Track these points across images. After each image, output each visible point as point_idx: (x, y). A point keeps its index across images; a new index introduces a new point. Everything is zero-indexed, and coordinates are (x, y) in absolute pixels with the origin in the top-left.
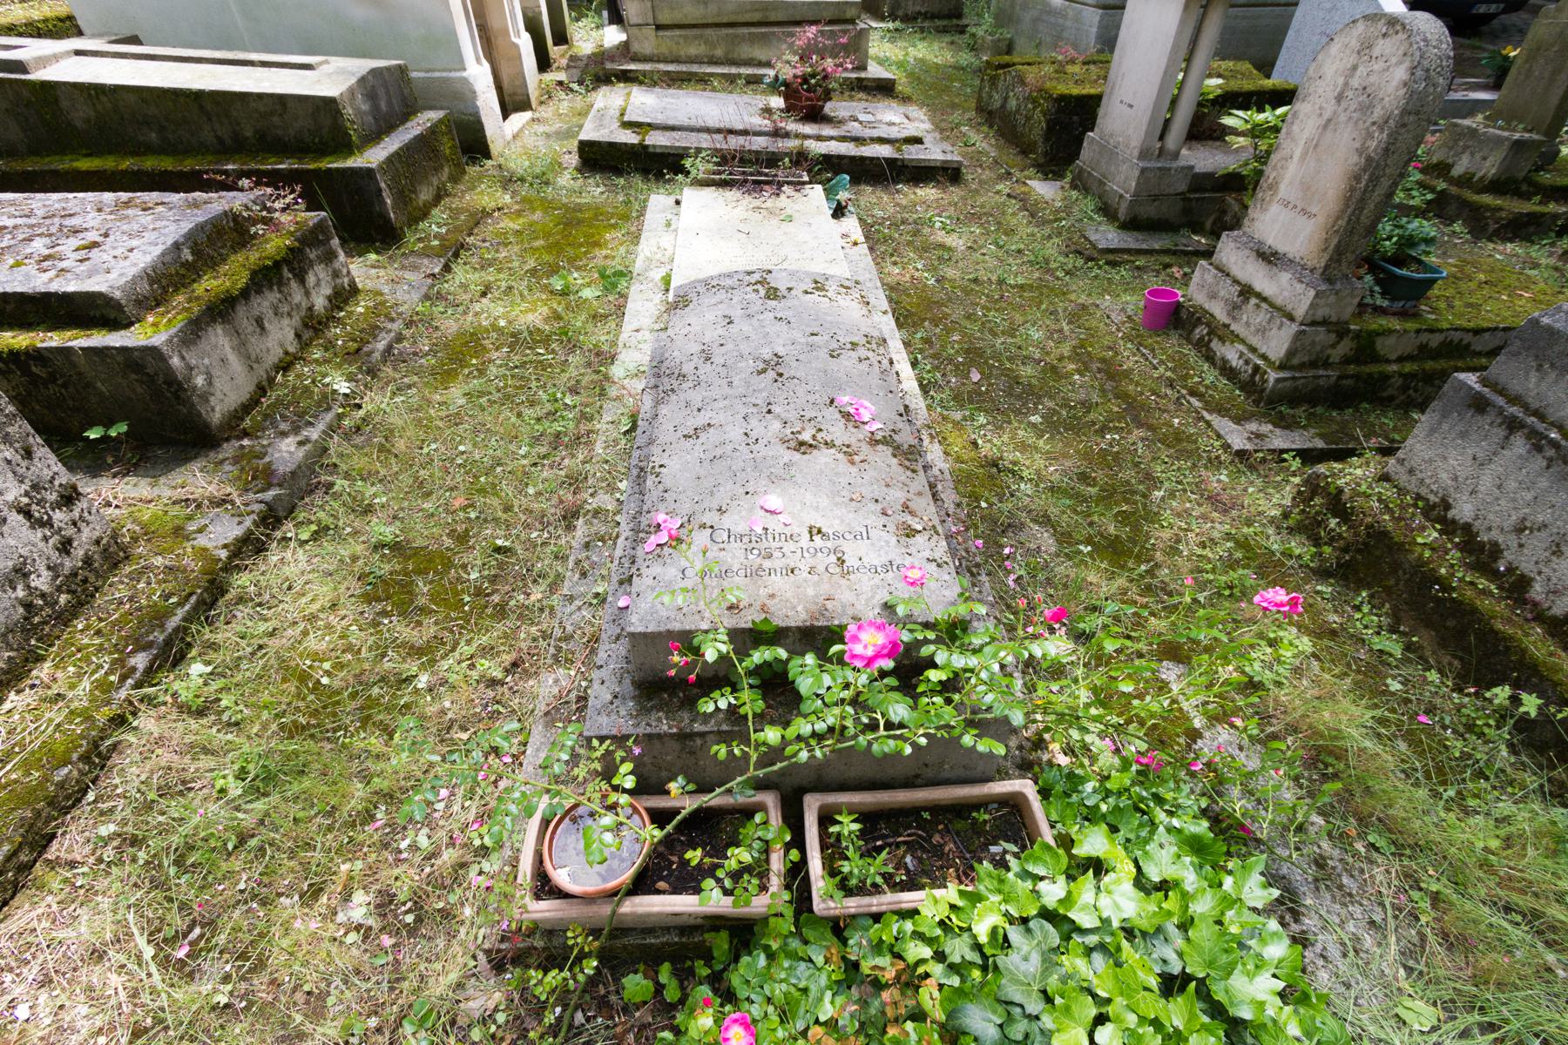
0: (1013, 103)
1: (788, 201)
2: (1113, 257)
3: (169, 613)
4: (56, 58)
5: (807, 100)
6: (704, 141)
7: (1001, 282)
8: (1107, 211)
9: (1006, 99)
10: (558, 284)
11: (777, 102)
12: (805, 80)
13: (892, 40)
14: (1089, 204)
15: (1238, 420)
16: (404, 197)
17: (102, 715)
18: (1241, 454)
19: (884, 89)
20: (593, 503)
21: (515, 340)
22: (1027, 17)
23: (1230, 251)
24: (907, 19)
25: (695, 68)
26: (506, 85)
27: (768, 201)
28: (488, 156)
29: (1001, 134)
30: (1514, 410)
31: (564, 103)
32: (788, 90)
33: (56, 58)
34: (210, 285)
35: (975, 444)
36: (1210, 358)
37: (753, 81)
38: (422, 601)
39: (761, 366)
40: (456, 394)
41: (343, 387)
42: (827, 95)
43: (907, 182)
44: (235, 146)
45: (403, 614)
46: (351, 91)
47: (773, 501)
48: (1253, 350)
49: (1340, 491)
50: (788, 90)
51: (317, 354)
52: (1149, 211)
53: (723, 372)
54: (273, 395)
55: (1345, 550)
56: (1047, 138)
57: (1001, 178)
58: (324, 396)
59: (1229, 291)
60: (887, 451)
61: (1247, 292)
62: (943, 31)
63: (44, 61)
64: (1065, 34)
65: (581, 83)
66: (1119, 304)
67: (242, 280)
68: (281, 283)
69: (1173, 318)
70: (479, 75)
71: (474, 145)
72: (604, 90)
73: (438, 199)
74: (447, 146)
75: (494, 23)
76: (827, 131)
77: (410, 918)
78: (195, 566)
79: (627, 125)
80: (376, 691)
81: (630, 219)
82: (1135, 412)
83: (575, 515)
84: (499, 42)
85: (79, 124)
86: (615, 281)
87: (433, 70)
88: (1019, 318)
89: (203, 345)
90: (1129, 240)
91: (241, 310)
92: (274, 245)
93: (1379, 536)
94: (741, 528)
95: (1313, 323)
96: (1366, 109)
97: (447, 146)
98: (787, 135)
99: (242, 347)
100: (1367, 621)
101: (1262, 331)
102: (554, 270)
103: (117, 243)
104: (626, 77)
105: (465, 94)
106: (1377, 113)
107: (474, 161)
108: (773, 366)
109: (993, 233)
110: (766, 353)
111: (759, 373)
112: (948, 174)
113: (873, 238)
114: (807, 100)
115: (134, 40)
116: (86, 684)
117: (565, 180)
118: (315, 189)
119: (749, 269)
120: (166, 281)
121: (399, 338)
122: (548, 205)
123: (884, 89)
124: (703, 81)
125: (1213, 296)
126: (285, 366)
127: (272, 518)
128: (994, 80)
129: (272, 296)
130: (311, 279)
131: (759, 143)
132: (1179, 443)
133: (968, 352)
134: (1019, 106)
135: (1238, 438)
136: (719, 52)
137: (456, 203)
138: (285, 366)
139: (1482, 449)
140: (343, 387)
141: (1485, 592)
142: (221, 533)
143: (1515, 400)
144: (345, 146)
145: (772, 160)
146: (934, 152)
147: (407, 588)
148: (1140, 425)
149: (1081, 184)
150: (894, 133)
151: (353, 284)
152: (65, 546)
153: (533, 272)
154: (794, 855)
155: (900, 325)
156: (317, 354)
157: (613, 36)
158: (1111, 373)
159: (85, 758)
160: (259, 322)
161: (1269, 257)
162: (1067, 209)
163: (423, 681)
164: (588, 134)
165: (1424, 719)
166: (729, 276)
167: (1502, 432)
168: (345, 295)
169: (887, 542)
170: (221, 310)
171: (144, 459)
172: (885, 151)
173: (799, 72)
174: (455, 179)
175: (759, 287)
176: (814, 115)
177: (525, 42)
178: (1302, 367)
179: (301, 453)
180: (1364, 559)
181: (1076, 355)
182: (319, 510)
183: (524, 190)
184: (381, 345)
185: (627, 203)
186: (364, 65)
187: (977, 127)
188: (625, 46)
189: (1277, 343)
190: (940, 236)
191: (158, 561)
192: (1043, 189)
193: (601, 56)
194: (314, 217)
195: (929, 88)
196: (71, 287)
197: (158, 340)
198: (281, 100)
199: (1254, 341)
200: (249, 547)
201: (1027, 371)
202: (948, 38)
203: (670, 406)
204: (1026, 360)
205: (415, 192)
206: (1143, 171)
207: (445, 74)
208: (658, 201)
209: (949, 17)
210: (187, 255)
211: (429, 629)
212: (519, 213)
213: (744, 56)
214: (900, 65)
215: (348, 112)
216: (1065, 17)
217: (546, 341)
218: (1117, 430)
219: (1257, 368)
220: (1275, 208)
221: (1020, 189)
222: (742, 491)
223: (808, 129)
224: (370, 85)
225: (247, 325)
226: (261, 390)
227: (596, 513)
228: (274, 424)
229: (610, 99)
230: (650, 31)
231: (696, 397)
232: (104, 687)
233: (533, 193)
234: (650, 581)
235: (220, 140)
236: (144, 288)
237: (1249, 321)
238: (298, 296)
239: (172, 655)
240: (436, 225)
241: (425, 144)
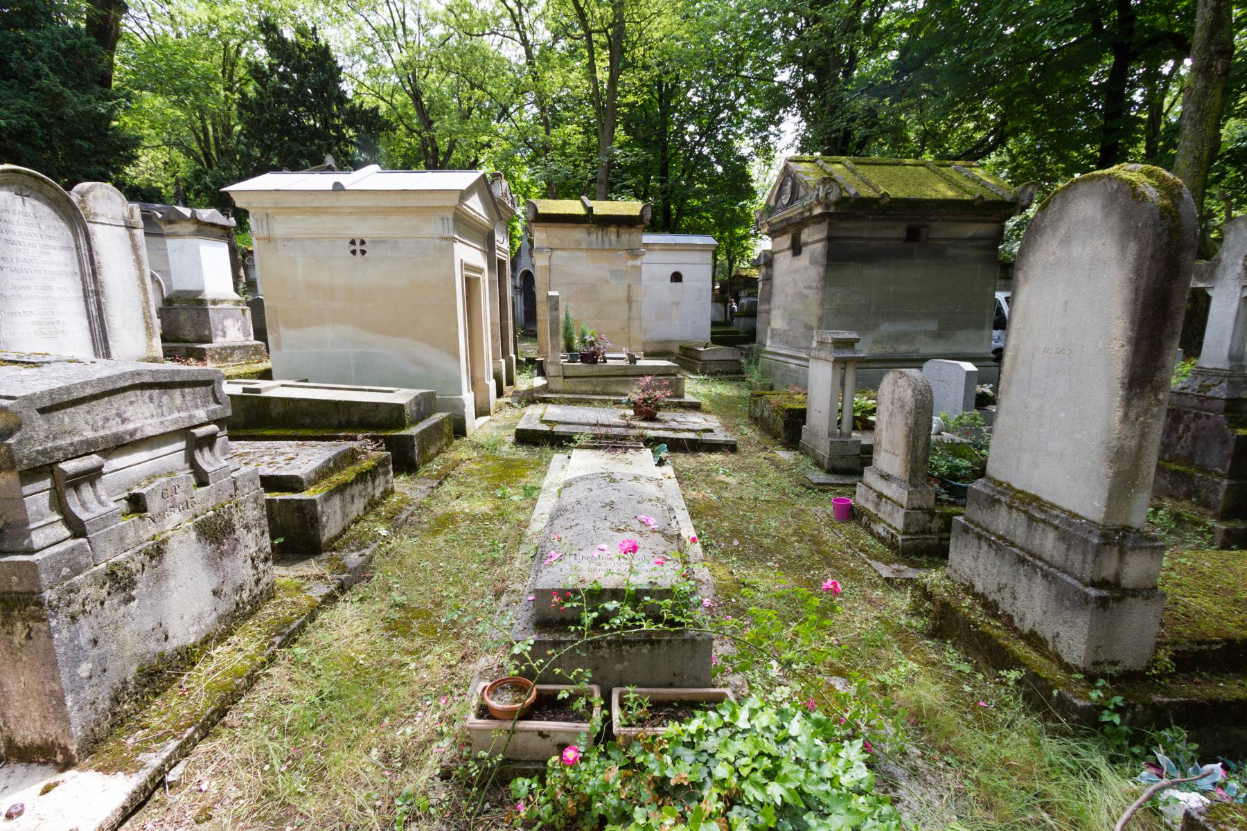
0: (766, 413)
1: (631, 455)
2: (823, 488)
3: (292, 621)
4: (273, 387)
5: (647, 411)
6: (587, 430)
7: (756, 499)
8: (818, 464)
10: (499, 493)
11: (631, 412)
12: (645, 400)
13: (703, 384)
14: (809, 461)
15: (887, 563)
16: (423, 450)
17: (259, 659)
18: (887, 579)
19: (695, 407)
20: (512, 587)
21: (473, 518)
22: (779, 373)
23: (869, 476)
24: (711, 374)
25: (585, 397)
27: (619, 455)
28: (464, 434)
29: (762, 429)
30: (978, 530)
31: (509, 412)
32: (635, 406)
33: (273, 387)
34: (338, 478)
35: (732, 573)
36: (872, 533)
37: (617, 403)
38: (414, 631)
40: (440, 540)
41: (384, 532)
42: (658, 408)
43: (705, 451)
44: (349, 425)
45: (404, 636)
46: (411, 402)
47: (604, 546)
48: (890, 526)
49: (925, 585)
50: (635, 406)
51: (372, 518)
52: (841, 464)
54: (349, 534)
55: (935, 619)
56: (785, 431)
57: (761, 450)
58: (374, 536)
59: (873, 496)
60: (660, 536)
61: (880, 495)
62: (734, 380)
63: (268, 389)
65: (519, 403)
66: (824, 508)
67: (353, 477)
68: (366, 481)
69: (849, 514)
70: (468, 398)
71: (459, 430)
72: (532, 406)
73: (438, 453)
74: (447, 429)
75: (478, 375)
76: (657, 425)
77: (399, 765)
78: (305, 603)
79: (543, 422)
80: (387, 669)
82: (828, 559)
83: (502, 593)
84: (479, 384)
85: (274, 415)
86: (531, 493)
88: (764, 515)
89: (331, 503)
90: (832, 479)
91: (348, 490)
92: (367, 464)
93: (945, 605)
94: (588, 555)
95: (914, 509)
96: (903, 407)
97: (447, 429)
98: (634, 427)
99: (343, 507)
100: (951, 656)
101: (891, 515)
102: (498, 487)
103: (303, 458)
104: (545, 401)
105: (460, 406)
106: (907, 409)
107: (457, 438)
108: (611, 505)
109: (756, 477)
110: (607, 501)
112: (732, 448)
113: (680, 477)
114: (647, 411)
115: (306, 381)
116: (253, 646)
117: (506, 448)
118: (391, 443)
120: (323, 473)
121: (412, 514)
122: (495, 459)
123: (695, 407)
124: (589, 403)
125: (867, 500)
126: (356, 522)
127: (343, 588)
128: (755, 402)
129: (361, 486)
130: (377, 482)
131: (616, 431)
132: (853, 575)
133: (732, 531)
135: (886, 572)
136: (598, 389)
137: (447, 456)
138: (356, 522)
139: (973, 552)
140: (384, 532)
141: (998, 628)
142: (319, 591)
143: (978, 525)
144: (402, 426)
145: (624, 438)
146: (720, 436)
147: (407, 625)
148: (830, 566)
149: (805, 451)
150: (696, 427)
151: (393, 488)
152: (257, 582)
153: (486, 488)
154: (605, 712)
155: (692, 518)
156: (372, 518)
157: (539, 382)
158: (815, 541)
159: (248, 678)
160: (353, 497)
161: (886, 477)
162: (797, 465)
163: (413, 666)
164: (522, 425)
165: (982, 704)
167: (976, 541)
168: (388, 493)
170: (341, 489)
171: (283, 558)
172: (691, 436)
173: (642, 396)
174: (447, 445)
176: (651, 418)
177: (492, 384)
178: (916, 533)
179: (361, 559)
180: (944, 623)
181: (795, 533)
182: (361, 589)
183: (483, 452)
184: (403, 517)
185: (541, 458)
186: (417, 392)
187: (748, 426)
188: (546, 386)
189: (898, 521)
190: (723, 478)
191: (289, 600)
192: (784, 455)
193: (531, 391)
194: (385, 454)
195: (722, 407)
196: (284, 473)
197: (316, 497)
198: (377, 405)
199: (889, 521)
200: (330, 599)
201: (767, 542)
202: (736, 383)
204: (767, 536)
206: (832, 443)
208: (558, 458)
209: (737, 373)
210: (331, 465)
211: (419, 642)
212: (480, 462)
214: (705, 396)
215: (407, 410)
217: (491, 519)
218: (818, 569)
219: (892, 535)
220: (883, 454)
221: (770, 455)
223: (651, 425)
224: (418, 400)
225: (348, 498)
226: (344, 530)
227: (513, 592)
228: (348, 547)
229: (536, 411)
230: (561, 379)
231: (572, 516)
232: (262, 647)
233: (488, 453)
235: (340, 422)
236: (313, 476)
237: (885, 510)
238: (370, 489)
239: (290, 640)
240: (435, 466)
241: (438, 426)
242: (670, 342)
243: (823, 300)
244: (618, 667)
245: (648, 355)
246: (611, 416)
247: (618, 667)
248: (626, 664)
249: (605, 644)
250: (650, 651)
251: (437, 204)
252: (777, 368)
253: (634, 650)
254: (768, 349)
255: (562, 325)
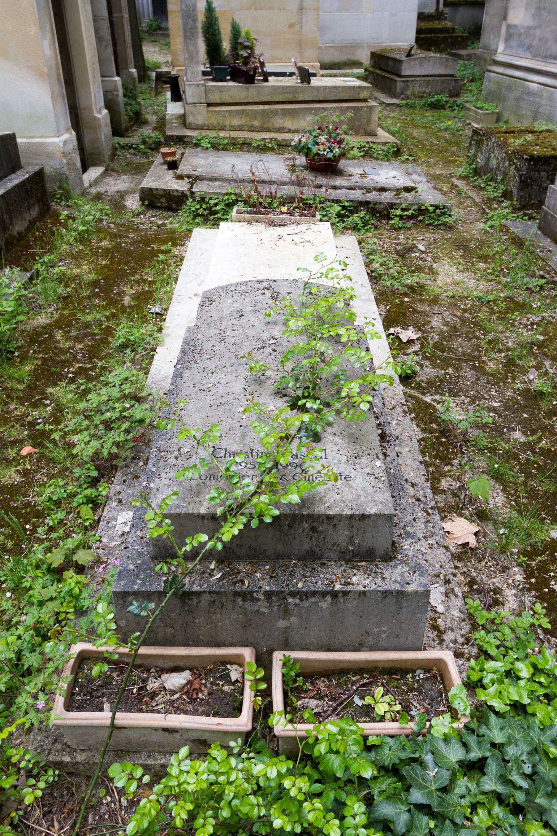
9: (488, 159)
26: (87, 146)
39: (261, 344)
53: (233, 348)
64: (541, 110)
81: (179, 238)
87: (33, 137)
111: (259, 349)
119: (260, 278)
134: (498, 164)
136: (256, 123)
166: (245, 283)
169: (339, 461)
175: (265, 291)
203: (192, 371)
205: (12, 223)
207: (41, 140)
213: (277, 126)
216: (540, 97)
222: (238, 425)
230: (203, 108)
231: (211, 365)
234: (167, 482)
242: (355, 46)
243: (194, 10)
244: (282, 624)
245: (329, 66)
246: (275, 167)
247: (282, 624)
248: (293, 619)
249: (261, 596)
250: (332, 604)
251: (334, 79)
252: (509, 88)
253: (306, 604)
254: (500, 57)
255: (201, 18)
